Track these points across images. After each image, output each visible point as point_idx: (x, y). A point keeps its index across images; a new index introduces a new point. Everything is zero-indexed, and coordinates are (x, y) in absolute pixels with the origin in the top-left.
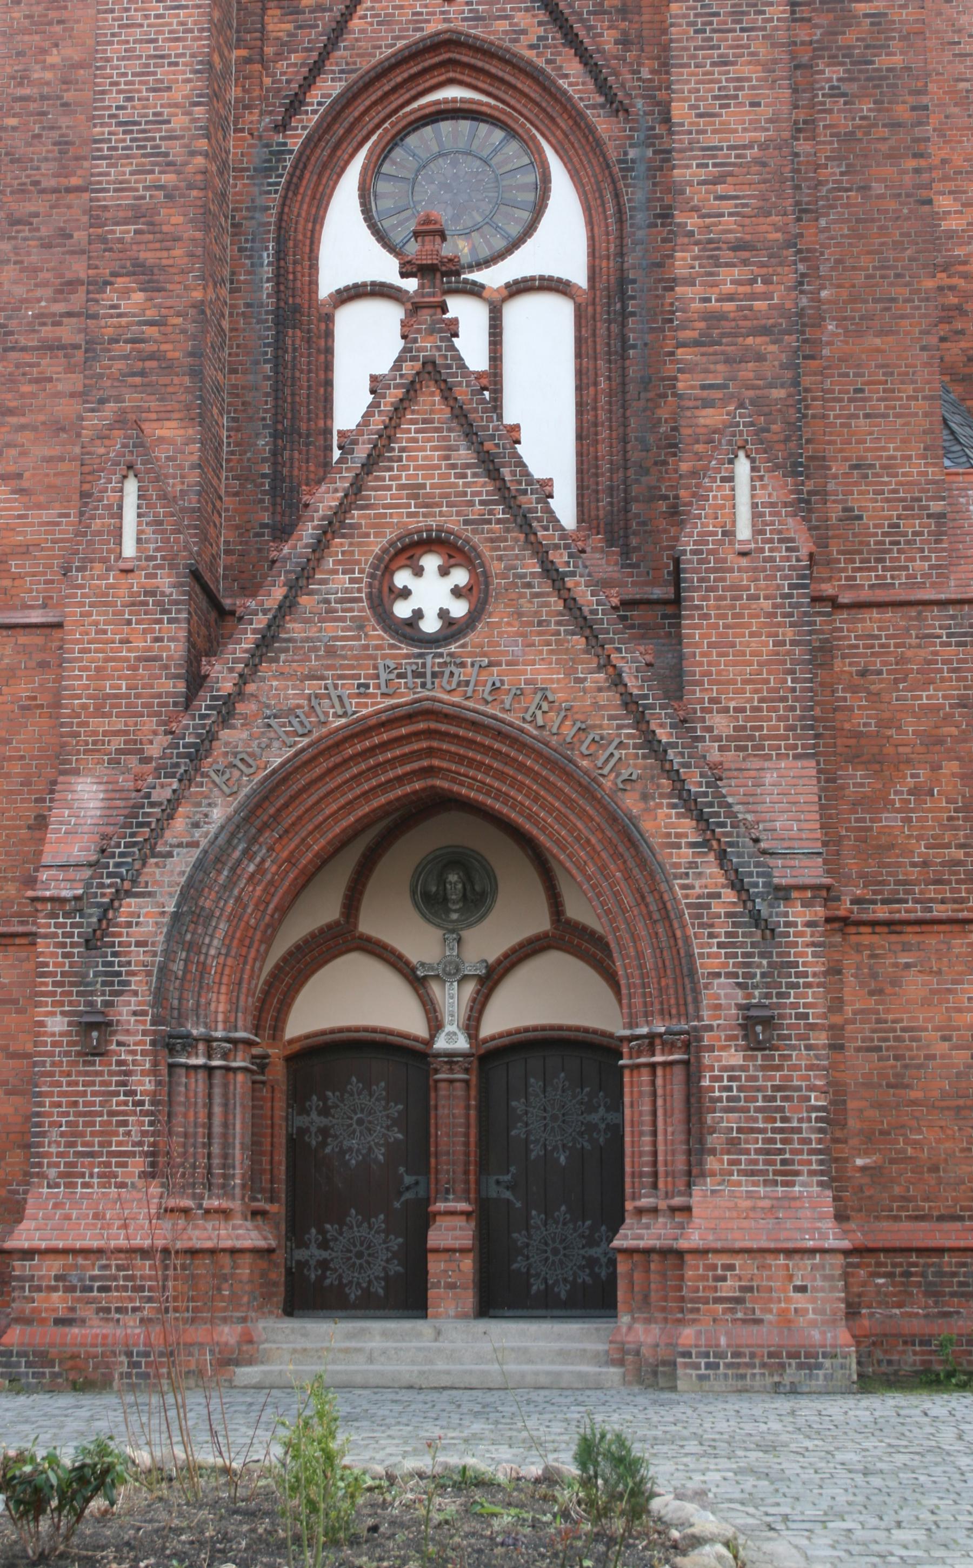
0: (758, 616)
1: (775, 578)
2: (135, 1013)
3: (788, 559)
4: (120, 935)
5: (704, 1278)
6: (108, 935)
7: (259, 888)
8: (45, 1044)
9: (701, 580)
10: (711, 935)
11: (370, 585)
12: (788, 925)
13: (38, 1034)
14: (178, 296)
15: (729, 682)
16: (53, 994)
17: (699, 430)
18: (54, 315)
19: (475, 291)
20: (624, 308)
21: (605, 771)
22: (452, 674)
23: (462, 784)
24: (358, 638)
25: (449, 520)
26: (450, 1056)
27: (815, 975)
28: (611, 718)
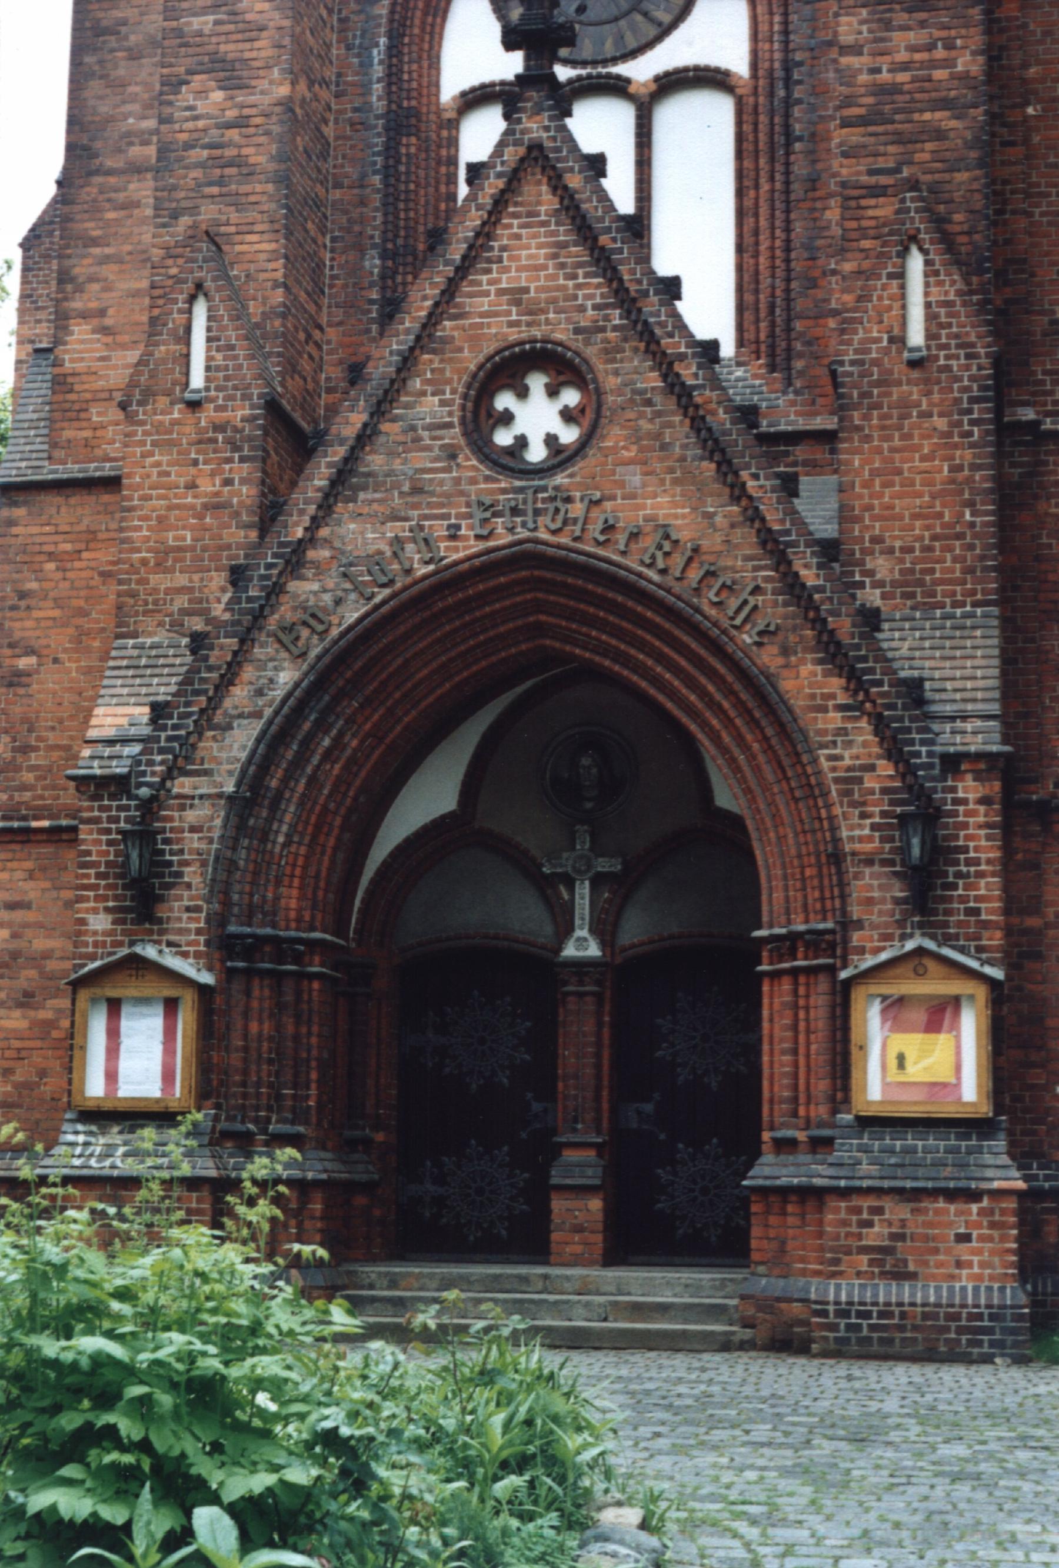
0: (929, 437)
1: (951, 390)
2: (188, 909)
3: (968, 368)
4: (171, 819)
5: (845, 1223)
6: (159, 820)
7: (337, 766)
8: (86, 945)
9: (863, 395)
10: (863, 816)
11: (463, 408)
12: (957, 802)
13: (79, 933)
14: (262, 93)
15: (894, 518)
16: (96, 887)
17: (865, 223)
18: (143, 132)
19: (618, 88)
20: (788, 96)
21: (738, 622)
22: (557, 510)
23: (575, 643)
24: (447, 470)
25: (560, 331)
26: (580, 966)
27: (989, 862)
28: (747, 558)
